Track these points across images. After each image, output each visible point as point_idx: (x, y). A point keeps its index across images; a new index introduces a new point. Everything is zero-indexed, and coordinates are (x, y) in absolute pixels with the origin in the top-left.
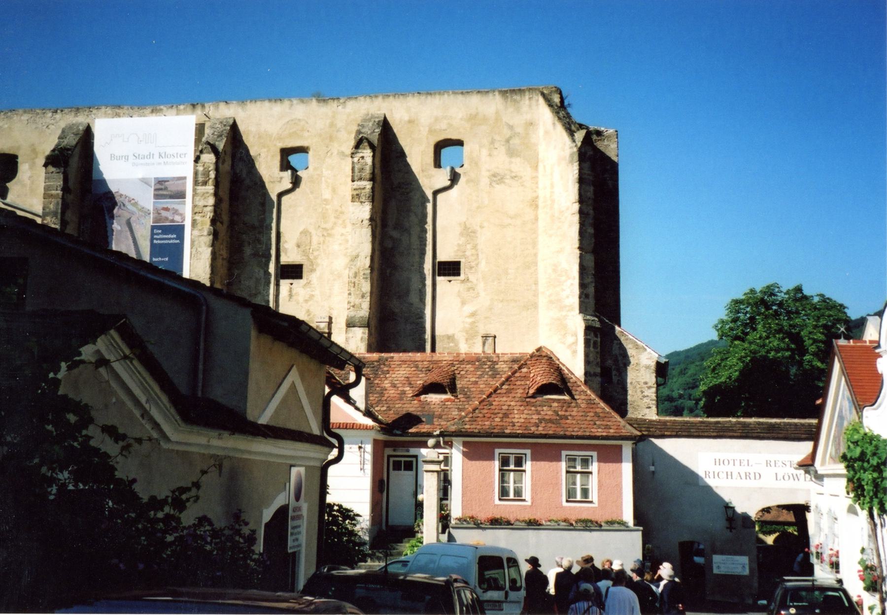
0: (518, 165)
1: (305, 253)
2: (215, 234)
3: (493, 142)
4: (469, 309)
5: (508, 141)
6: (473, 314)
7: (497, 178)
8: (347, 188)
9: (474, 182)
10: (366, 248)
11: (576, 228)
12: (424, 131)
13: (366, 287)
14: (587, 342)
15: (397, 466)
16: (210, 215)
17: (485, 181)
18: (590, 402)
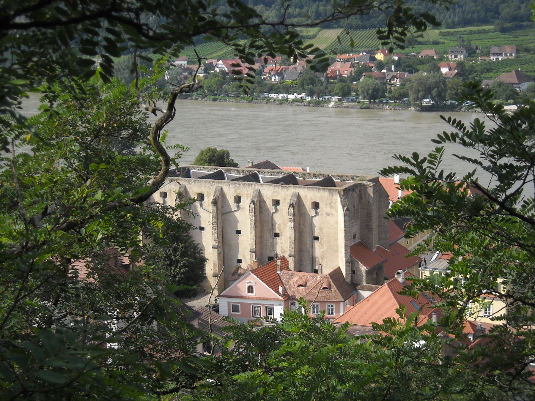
0: (333, 211)
1: (280, 230)
2: (255, 227)
3: (326, 204)
4: (322, 250)
5: (330, 204)
6: (323, 252)
7: (328, 214)
8: (287, 217)
9: (322, 215)
10: (293, 236)
11: (344, 235)
12: (309, 199)
13: (293, 246)
14: (346, 266)
15: (292, 304)
16: (254, 222)
17: (325, 215)
18: (335, 291)
